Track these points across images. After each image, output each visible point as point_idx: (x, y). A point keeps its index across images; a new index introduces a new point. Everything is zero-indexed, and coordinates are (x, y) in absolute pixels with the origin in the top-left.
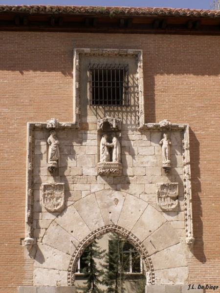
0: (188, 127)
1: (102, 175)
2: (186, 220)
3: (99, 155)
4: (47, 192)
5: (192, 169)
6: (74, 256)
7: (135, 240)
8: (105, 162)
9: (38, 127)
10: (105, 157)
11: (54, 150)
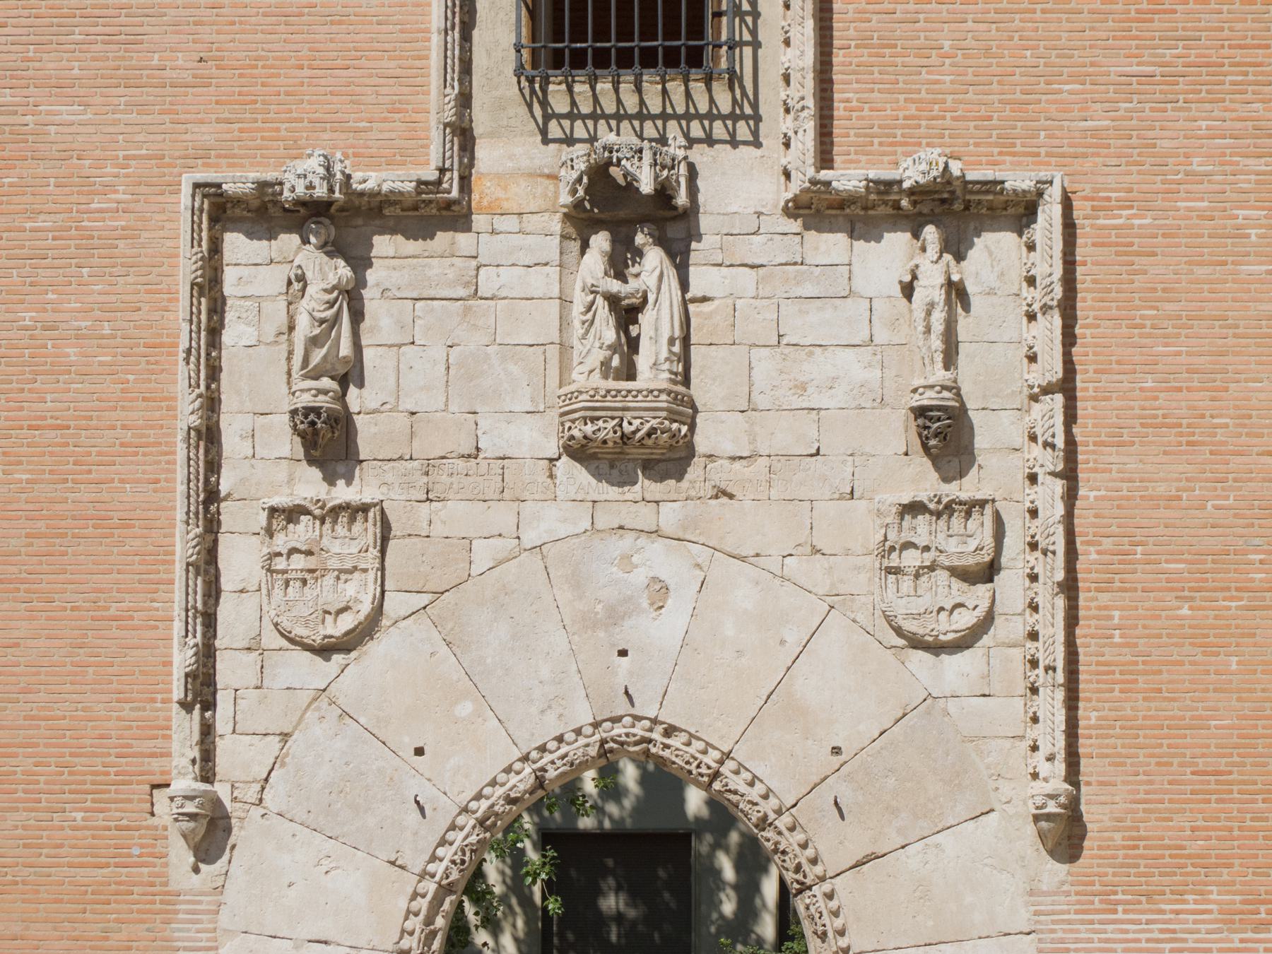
0: (1053, 194)
1: (580, 452)
2: (1034, 690)
3: (565, 348)
4: (281, 542)
6: (424, 875)
7: (755, 793)
8: (597, 381)
9: (237, 201)
10: (599, 356)
11: (322, 321)
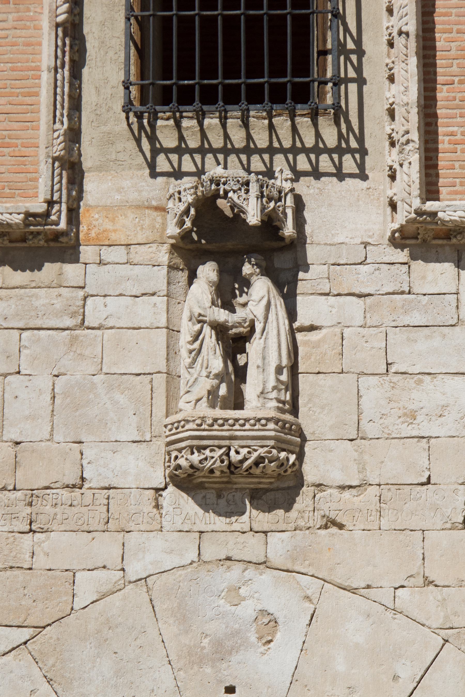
5: (242, 114)
